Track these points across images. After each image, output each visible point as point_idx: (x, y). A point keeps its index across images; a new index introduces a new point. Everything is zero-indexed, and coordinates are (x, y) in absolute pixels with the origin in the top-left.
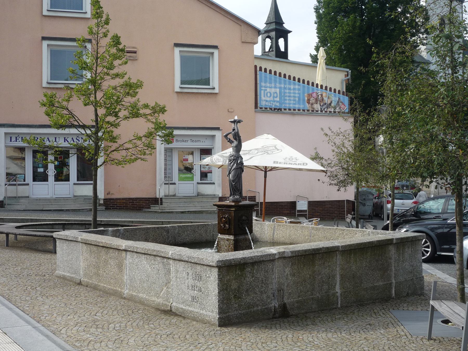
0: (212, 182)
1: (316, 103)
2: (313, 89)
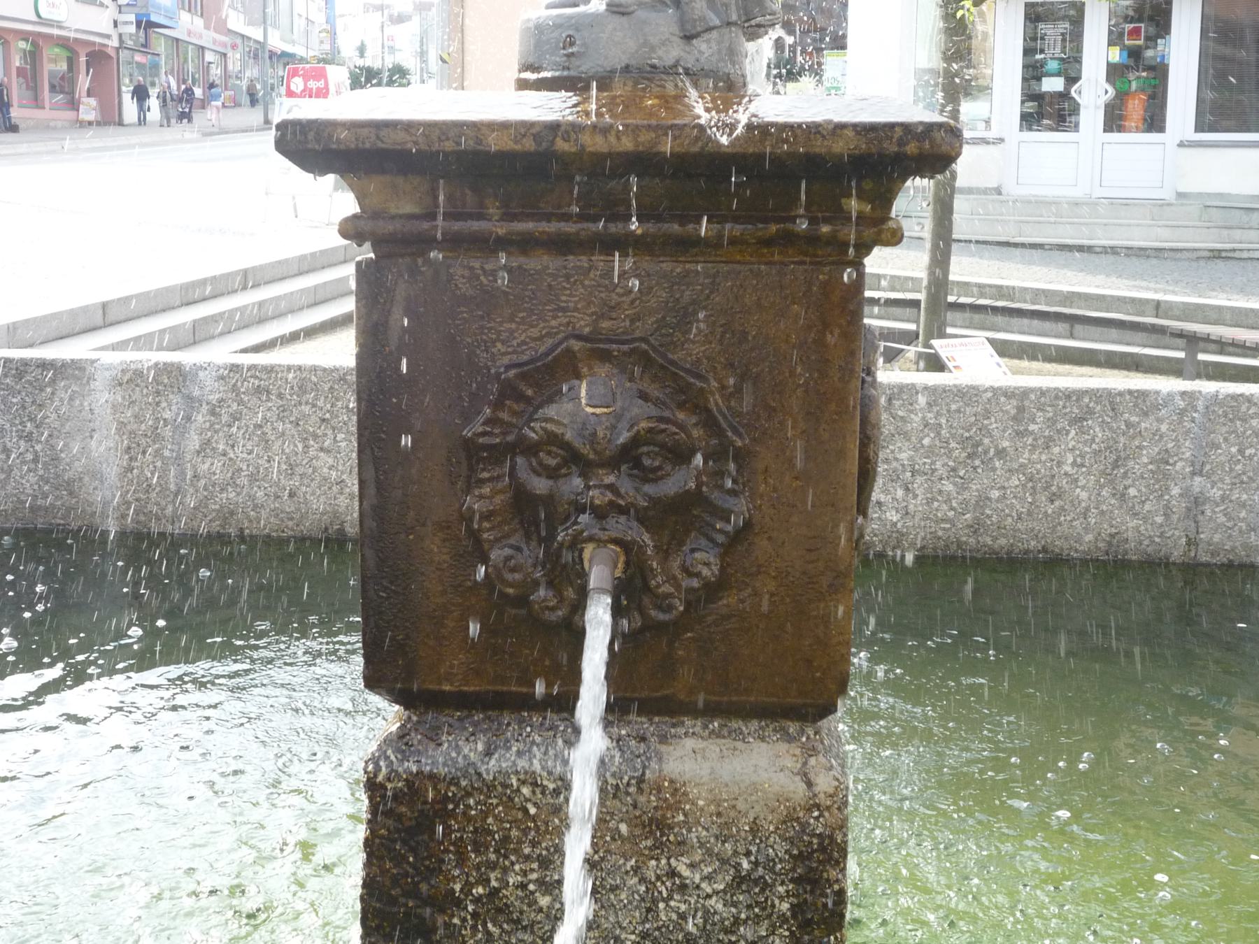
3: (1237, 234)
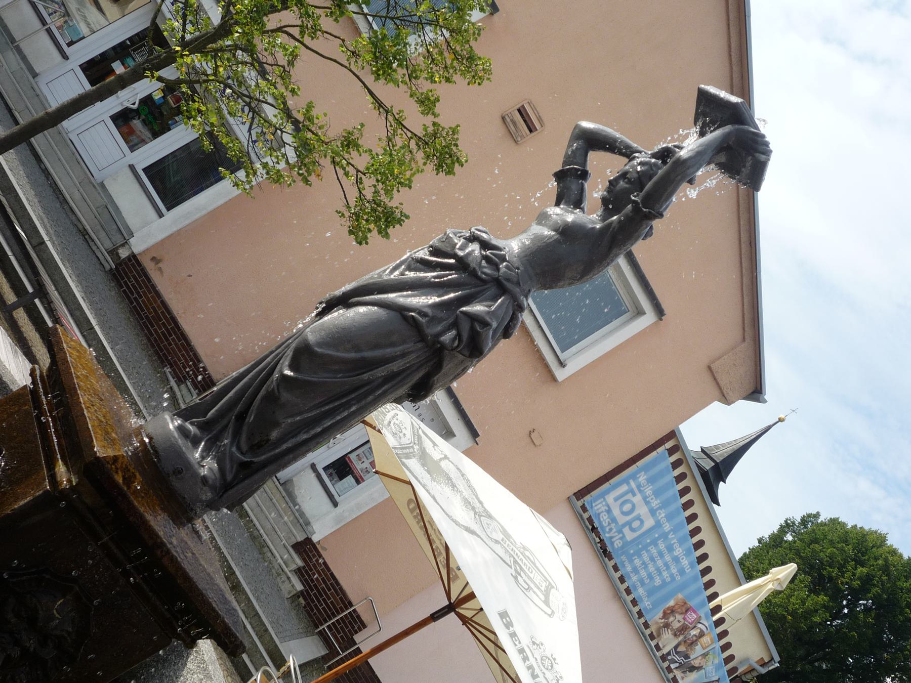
0: (336, 496)
1: (675, 635)
2: (702, 605)
3: (102, 234)
